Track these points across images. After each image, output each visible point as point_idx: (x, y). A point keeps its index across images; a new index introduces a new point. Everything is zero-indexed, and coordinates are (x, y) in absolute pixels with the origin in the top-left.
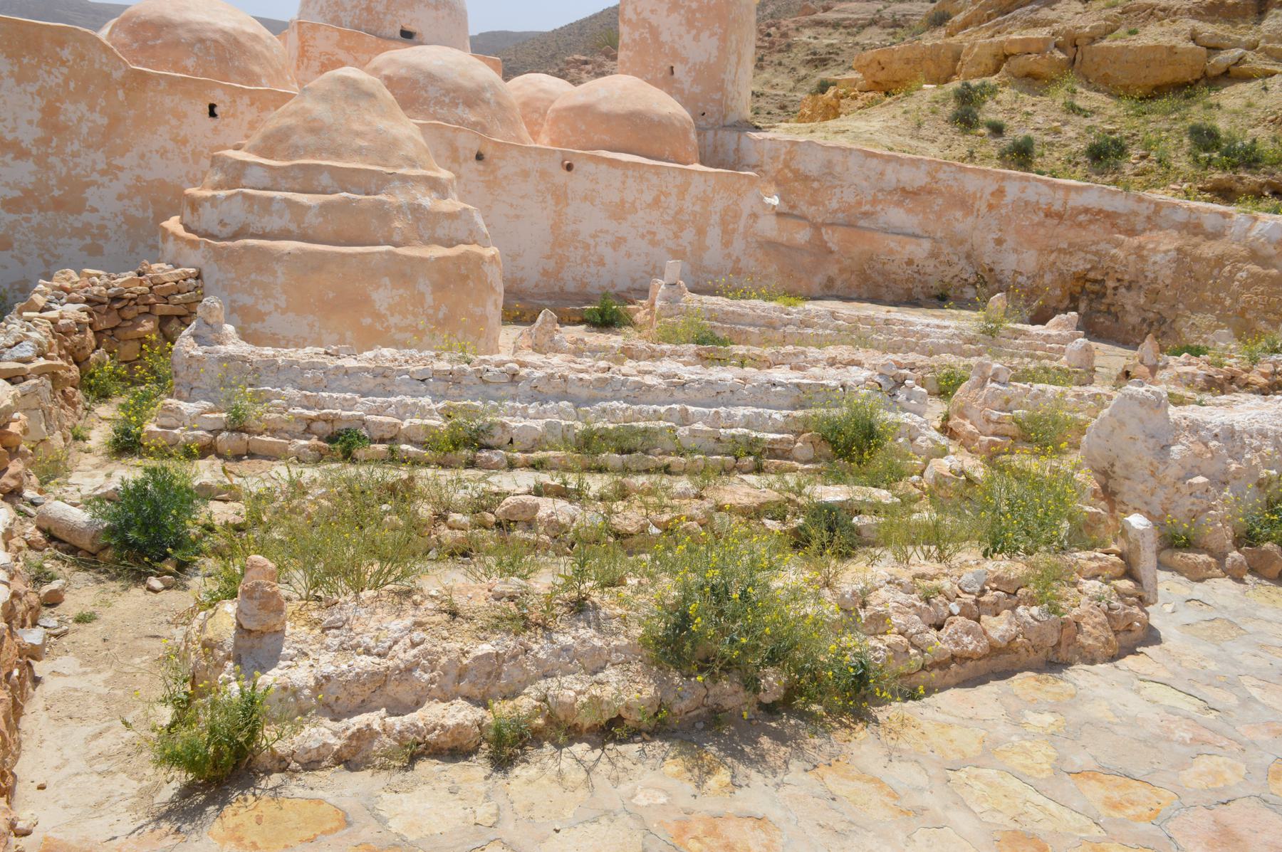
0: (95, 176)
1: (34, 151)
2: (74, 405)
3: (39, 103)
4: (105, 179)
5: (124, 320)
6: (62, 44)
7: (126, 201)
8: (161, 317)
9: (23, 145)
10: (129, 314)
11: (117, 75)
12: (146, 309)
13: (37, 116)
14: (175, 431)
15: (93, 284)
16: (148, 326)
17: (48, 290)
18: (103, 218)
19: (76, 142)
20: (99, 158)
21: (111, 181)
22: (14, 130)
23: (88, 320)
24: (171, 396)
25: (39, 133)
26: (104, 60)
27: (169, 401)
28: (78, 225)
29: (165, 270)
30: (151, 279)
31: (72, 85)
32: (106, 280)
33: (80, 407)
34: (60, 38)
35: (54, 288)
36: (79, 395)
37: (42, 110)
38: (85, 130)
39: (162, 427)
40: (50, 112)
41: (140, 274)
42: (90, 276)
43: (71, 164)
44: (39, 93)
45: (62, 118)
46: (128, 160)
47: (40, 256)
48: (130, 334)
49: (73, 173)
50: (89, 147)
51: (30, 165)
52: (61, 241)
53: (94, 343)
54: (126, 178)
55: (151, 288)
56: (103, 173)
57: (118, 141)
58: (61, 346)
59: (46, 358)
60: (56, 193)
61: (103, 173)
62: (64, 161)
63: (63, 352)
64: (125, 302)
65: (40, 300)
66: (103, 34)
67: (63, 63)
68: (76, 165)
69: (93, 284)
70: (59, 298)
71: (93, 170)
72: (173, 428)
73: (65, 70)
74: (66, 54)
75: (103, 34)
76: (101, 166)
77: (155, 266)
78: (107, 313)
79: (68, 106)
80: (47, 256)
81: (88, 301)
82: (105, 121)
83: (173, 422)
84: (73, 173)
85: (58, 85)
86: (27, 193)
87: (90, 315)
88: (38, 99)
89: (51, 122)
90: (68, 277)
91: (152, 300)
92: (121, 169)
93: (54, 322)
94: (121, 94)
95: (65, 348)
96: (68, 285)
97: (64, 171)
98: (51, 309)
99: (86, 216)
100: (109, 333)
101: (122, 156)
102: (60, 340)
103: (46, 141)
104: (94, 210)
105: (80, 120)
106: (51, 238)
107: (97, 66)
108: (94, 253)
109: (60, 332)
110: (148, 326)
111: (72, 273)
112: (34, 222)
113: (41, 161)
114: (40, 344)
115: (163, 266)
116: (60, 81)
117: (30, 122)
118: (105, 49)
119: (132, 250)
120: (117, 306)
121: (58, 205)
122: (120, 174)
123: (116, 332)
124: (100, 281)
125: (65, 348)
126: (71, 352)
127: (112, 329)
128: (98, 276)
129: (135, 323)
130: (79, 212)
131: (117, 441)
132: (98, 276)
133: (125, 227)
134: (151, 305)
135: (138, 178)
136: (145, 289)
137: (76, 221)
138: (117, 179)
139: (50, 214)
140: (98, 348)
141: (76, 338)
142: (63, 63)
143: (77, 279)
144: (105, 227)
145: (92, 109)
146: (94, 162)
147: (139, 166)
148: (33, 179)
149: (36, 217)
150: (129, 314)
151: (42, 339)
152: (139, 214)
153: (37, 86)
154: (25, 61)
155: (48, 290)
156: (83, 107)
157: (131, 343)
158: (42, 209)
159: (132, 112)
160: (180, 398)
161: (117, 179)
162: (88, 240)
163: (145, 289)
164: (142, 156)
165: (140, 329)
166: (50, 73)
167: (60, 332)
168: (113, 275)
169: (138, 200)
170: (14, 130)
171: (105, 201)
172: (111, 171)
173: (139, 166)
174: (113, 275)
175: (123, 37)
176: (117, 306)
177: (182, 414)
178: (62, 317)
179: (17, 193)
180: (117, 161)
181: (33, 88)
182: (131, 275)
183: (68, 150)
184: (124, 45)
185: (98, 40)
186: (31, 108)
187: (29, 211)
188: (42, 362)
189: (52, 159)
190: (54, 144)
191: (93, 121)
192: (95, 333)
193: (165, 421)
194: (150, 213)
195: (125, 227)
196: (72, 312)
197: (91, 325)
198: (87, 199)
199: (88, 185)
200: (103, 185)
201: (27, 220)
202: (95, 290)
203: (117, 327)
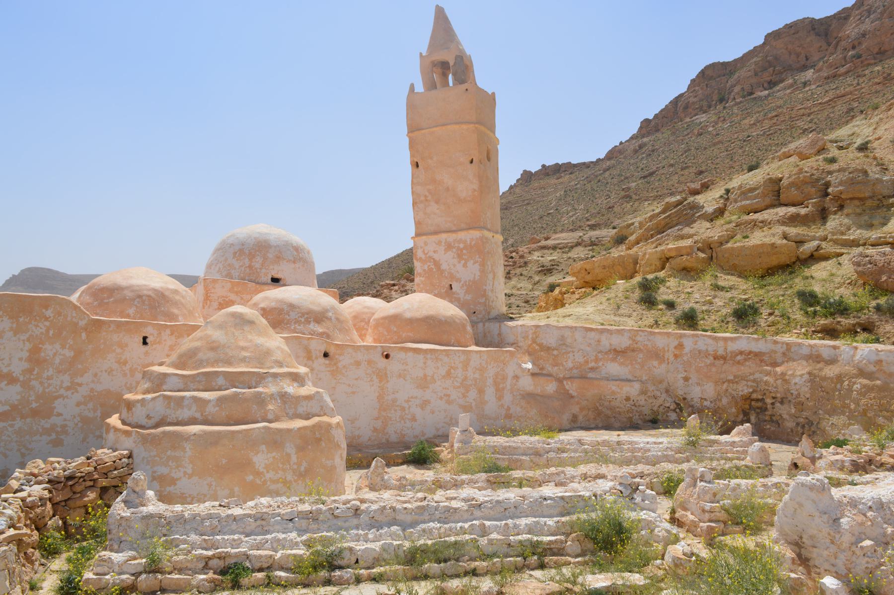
0: (62, 392)
1: (21, 378)
2: (32, 562)
3: (28, 346)
4: (69, 393)
5: (74, 493)
6: (46, 307)
7: (82, 407)
8: (101, 488)
9: (14, 375)
10: (78, 488)
11: (82, 323)
12: (91, 483)
13: (25, 354)
14: (107, 577)
15: (54, 469)
16: (92, 495)
17: (22, 476)
18: (65, 420)
19: (51, 369)
20: (66, 379)
21: (73, 393)
22: (9, 365)
23: (48, 496)
24: (105, 549)
25: (26, 365)
26: (74, 315)
27: (104, 553)
28: (47, 426)
29: (106, 454)
30: (96, 461)
31: (51, 332)
32: (64, 465)
33: (37, 563)
34: (46, 303)
35: (26, 474)
36: (37, 554)
37: (30, 351)
38: (57, 361)
39: (97, 574)
40: (35, 350)
41: (88, 458)
42: (52, 463)
43: (46, 385)
44: (28, 340)
45: (43, 354)
46: (86, 378)
47: (19, 450)
48: (79, 503)
49: (47, 390)
50: (59, 372)
51: (17, 388)
52: (35, 438)
53: (51, 513)
54: (83, 391)
55: (95, 468)
56: (68, 389)
57: (80, 366)
58: (27, 517)
59: (15, 528)
60: (34, 405)
61: (68, 389)
62: (41, 383)
63: (28, 522)
64: (76, 480)
65: (14, 484)
66: (74, 298)
67: (47, 319)
68: (49, 385)
69: (54, 469)
70: (29, 481)
71: (61, 387)
72: (105, 574)
73: (47, 324)
74: (49, 313)
75: (74, 298)
76: (67, 384)
77: (99, 451)
78: (63, 489)
79: (47, 346)
80: (23, 450)
81: (50, 482)
82: (72, 354)
83: (106, 569)
84: (47, 390)
85: (42, 333)
86: (14, 407)
87: (50, 492)
88: (27, 344)
89: (36, 359)
90: (37, 465)
91: (96, 476)
92: (80, 385)
93: (23, 500)
94: (84, 335)
95: (30, 519)
96: (36, 471)
97: (41, 390)
98: (22, 490)
99: (55, 420)
100: (63, 504)
101: (82, 376)
102: (27, 513)
103: (30, 371)
104: (59, 415)
105: (55, 354)
106: (27, 437)
107: (69, 319)
108: (57, 445)
109: (27, 507)
110: (92, 495)
111: (39, 462)
112: (17, 427)
113: (26, 385)
114: (11, 518)
115: (106, 450)
116: (43, 331)
117: (21, 359)
118: (76, 307)
119: (84, 440)
120: (70, 483)
121: (35, 413)
122: (79, 389)
123: (68, 502)
124: (59, 466)
125: (30, 519)
126: (33, 521)
127: (65, 501)
128: (59, 463)
129: (83, 494)
130: (49, 418)
131: (62, 588)
132: (59, 463)
133: (80, 425)
134: (95, 481)
135: (92, 390)
136: (91, 469)
137: (46, 424)
138: (77, 392)
139: (28, 420)
140: (54, 516)
141: (38, 510)
142: (47, 319)
143: (43, 466)
144: (66, 426)
145: (63, 347)
146: (62, 382)
147: (93, 382)
148: (19, 397)
149: (18, 423)
150: (78, 488)
151: (14, 514)
152: (91, 415)
153: (27, 335)
154: (21, 320)
155: (22, 476)
156: (57, 346)
157: (78, 510)
158: (23, 417)
159: (90, 347)
160: (111, 551)
161: (77, 392)
162: (54, 436)
163: (91, 469)
164: (96, 375)
165: (86, 499)
166: (37, 326)
167: (27, 507)
168: (69, 461)
169: (91, 405)
170: (9, 365)
171: (68, 408)
172: (73, 387)
173: (93, 382)
174: (69, 461)
175: (88, 299)
176: (70, 483)
177: (112, 563)
178: (30, 496)
179: (7, 408)
180: (79, 380)
181: (24, 337)
182: (82, 459)
183: (45, 375)
184: (88, 304)
185: (71, 302)
186: (22, 350)
187: (14, 419)
188: (12, 532)
189: (33, 383)
190: (35, 372)
191: (64, 355)
192: (53, 505)
193: (99, 570)
194: (99, 414)
195: (80, 425)
196: (37, 491)
197: (50, 499)
198: (55, 407)
199: (57, 398)
200: (67, 397)
201: (12, 426)
202: (55, 473)
203: (69, 499)
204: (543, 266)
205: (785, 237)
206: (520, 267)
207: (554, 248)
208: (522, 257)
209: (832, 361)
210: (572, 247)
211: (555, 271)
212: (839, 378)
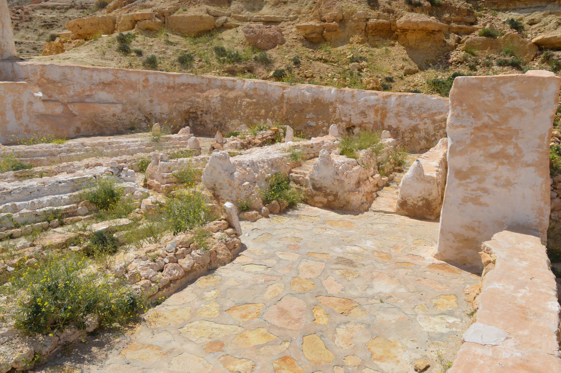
204: (45, 22)
205: (208, 12)
206: (26, 21)
207: (53, 8)
208: (27, 13)
209: (232, 89)
210: (67, 9)
211: (55, 26)
212: (236, 98)
